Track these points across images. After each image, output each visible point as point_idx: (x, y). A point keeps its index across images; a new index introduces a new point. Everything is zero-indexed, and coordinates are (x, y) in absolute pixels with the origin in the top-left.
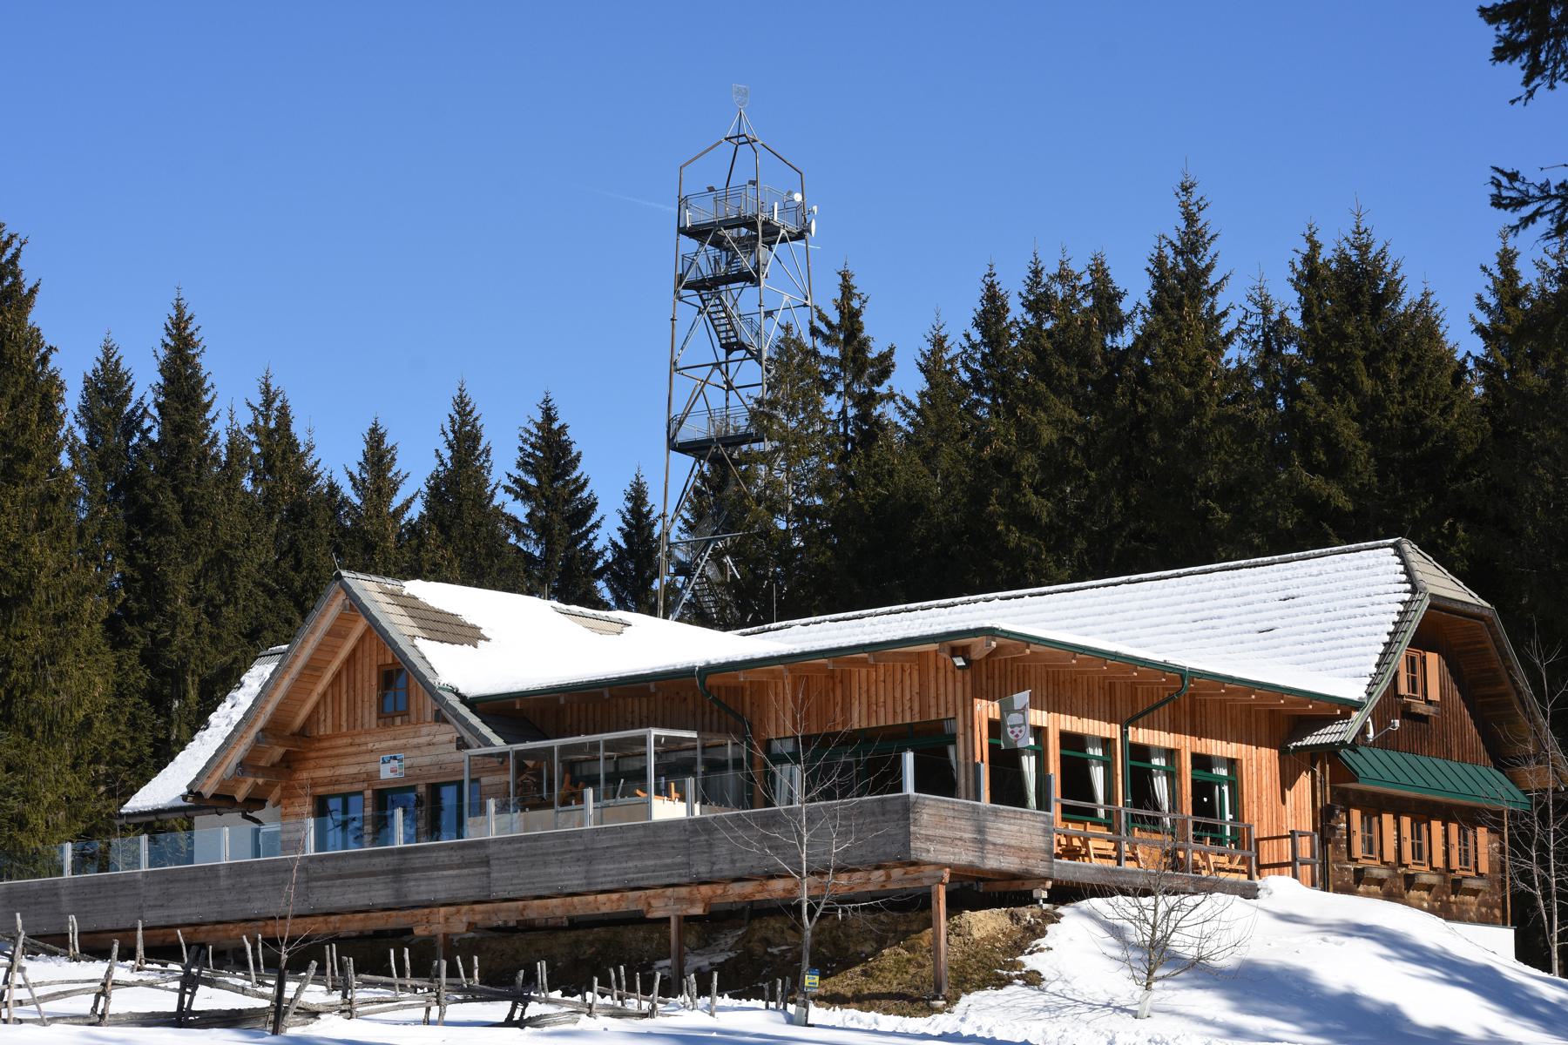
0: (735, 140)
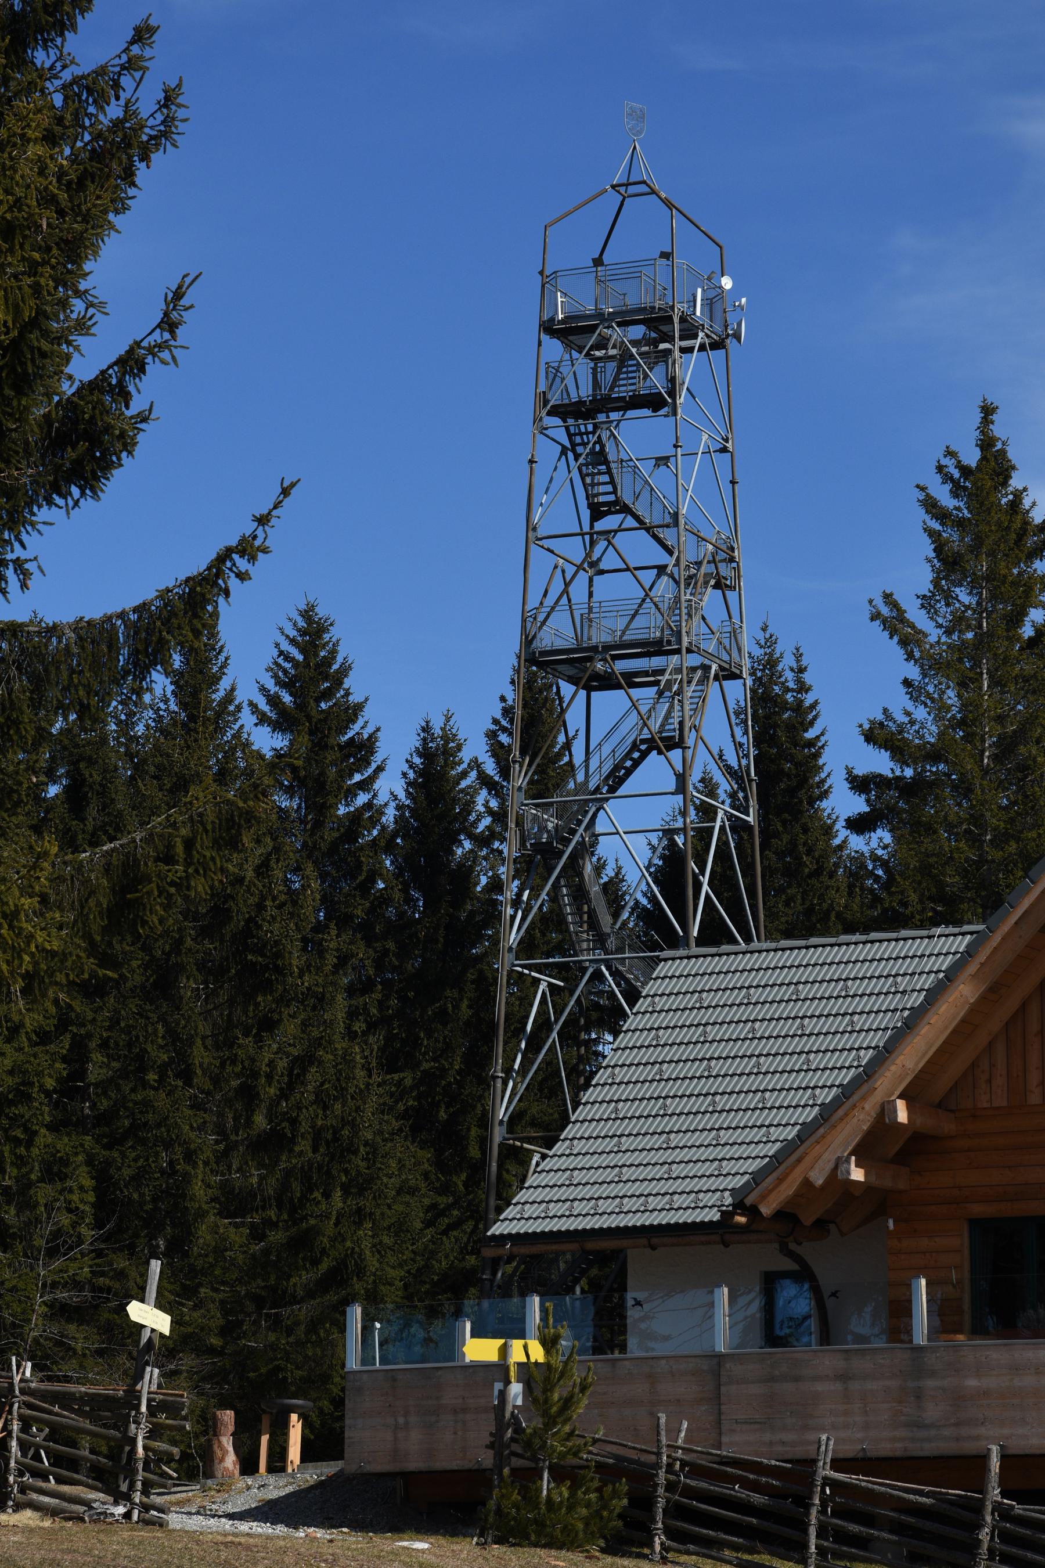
0: (622, 190)
